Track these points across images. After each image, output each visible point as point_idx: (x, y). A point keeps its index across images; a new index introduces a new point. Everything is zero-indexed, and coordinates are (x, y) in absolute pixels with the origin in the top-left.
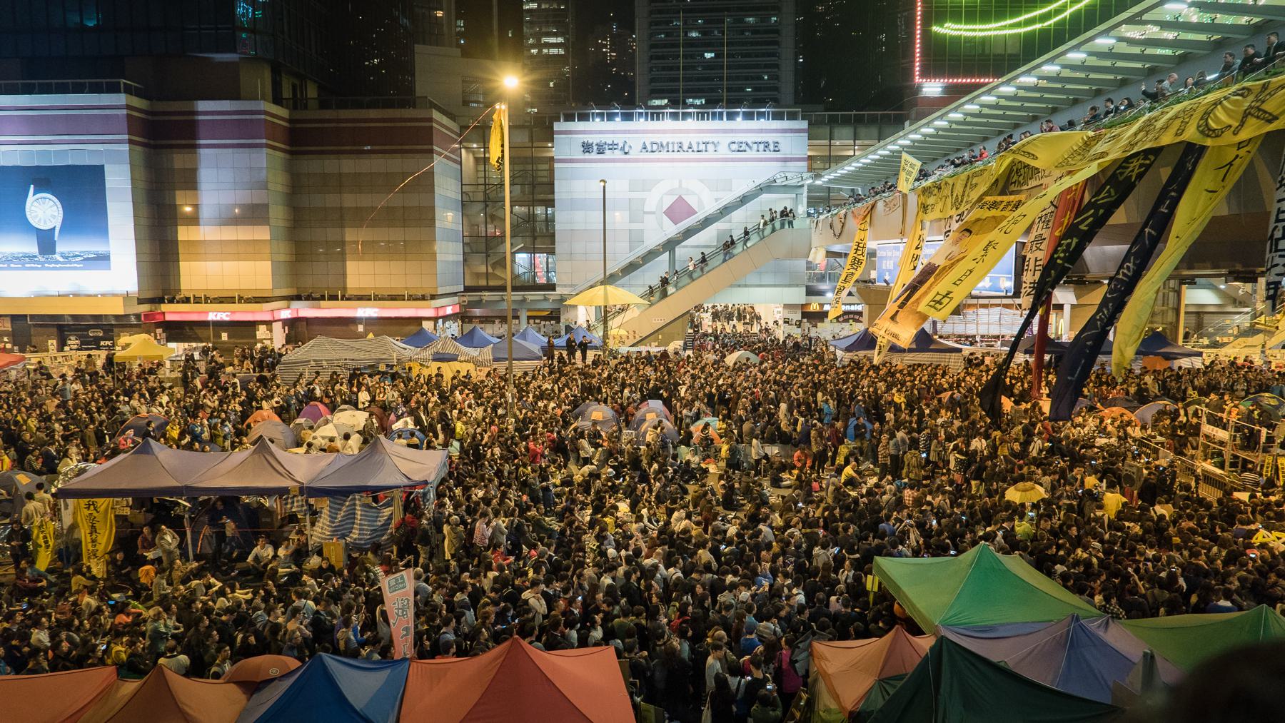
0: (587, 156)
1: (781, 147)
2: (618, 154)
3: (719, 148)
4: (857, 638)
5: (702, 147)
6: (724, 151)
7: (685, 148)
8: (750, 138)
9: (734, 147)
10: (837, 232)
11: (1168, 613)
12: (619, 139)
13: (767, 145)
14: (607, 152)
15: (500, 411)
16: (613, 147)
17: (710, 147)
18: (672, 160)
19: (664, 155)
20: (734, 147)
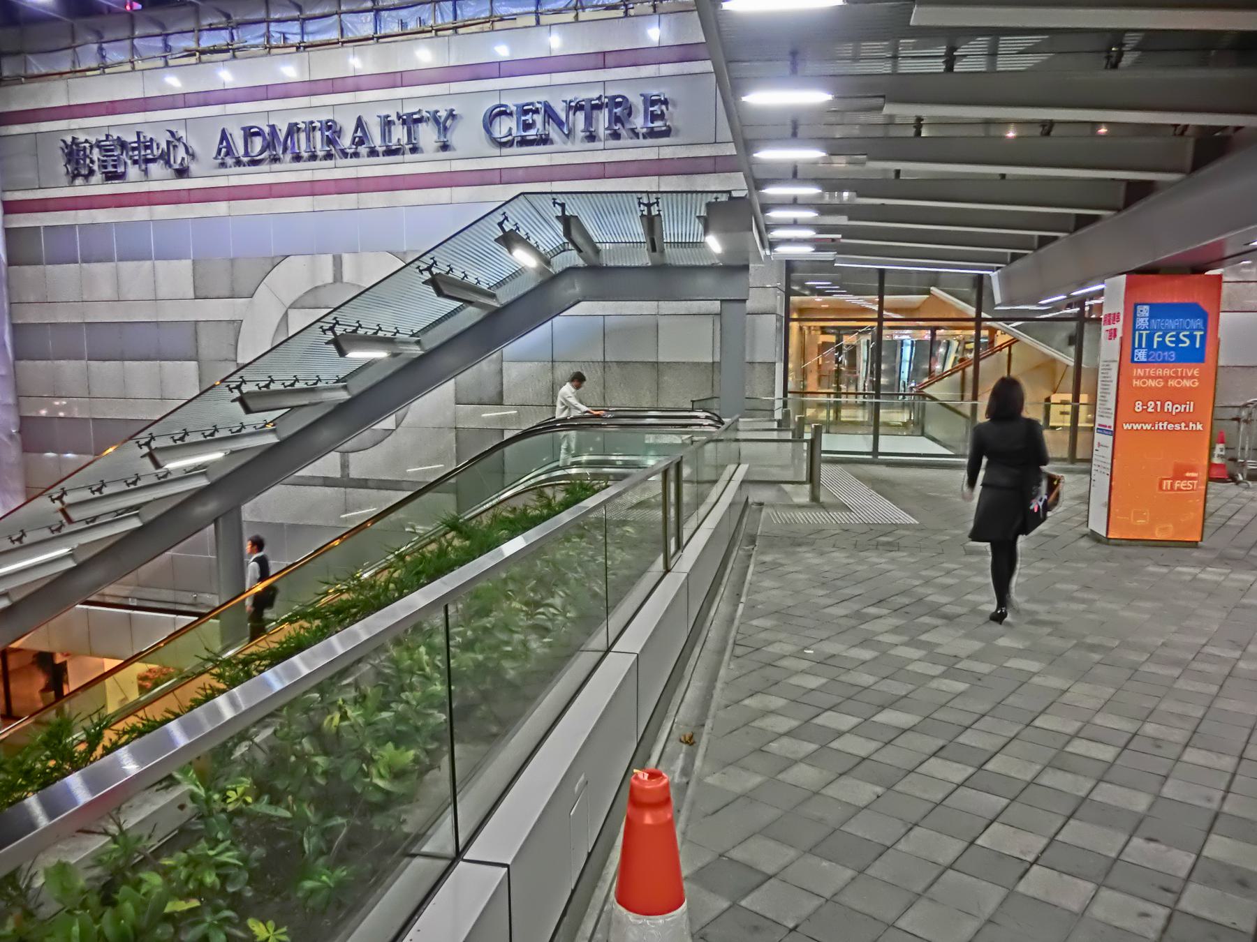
0: (80, 189)
1: (675, 117)
2: (160, 179)
3: (454, 138)
4: (72, 227)
5: (399, 134)
6: (468, 135)
7: (346, 142)
8: (561, 90)
9: (504, 127)
10: (1113, 60)
11: (271, 803)
12: (154, 125)
13: (619, 110)
14: (133, 172)
15: (210, 879)
16: (143, 153)
17: (427, 135)
18: (312, 189)
19: (287, 172)
20: (504, 127)
